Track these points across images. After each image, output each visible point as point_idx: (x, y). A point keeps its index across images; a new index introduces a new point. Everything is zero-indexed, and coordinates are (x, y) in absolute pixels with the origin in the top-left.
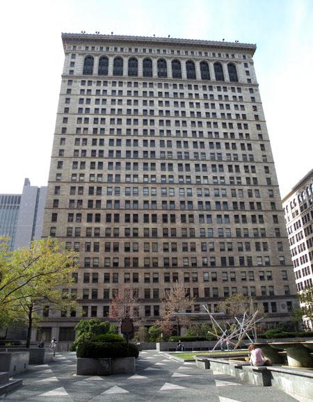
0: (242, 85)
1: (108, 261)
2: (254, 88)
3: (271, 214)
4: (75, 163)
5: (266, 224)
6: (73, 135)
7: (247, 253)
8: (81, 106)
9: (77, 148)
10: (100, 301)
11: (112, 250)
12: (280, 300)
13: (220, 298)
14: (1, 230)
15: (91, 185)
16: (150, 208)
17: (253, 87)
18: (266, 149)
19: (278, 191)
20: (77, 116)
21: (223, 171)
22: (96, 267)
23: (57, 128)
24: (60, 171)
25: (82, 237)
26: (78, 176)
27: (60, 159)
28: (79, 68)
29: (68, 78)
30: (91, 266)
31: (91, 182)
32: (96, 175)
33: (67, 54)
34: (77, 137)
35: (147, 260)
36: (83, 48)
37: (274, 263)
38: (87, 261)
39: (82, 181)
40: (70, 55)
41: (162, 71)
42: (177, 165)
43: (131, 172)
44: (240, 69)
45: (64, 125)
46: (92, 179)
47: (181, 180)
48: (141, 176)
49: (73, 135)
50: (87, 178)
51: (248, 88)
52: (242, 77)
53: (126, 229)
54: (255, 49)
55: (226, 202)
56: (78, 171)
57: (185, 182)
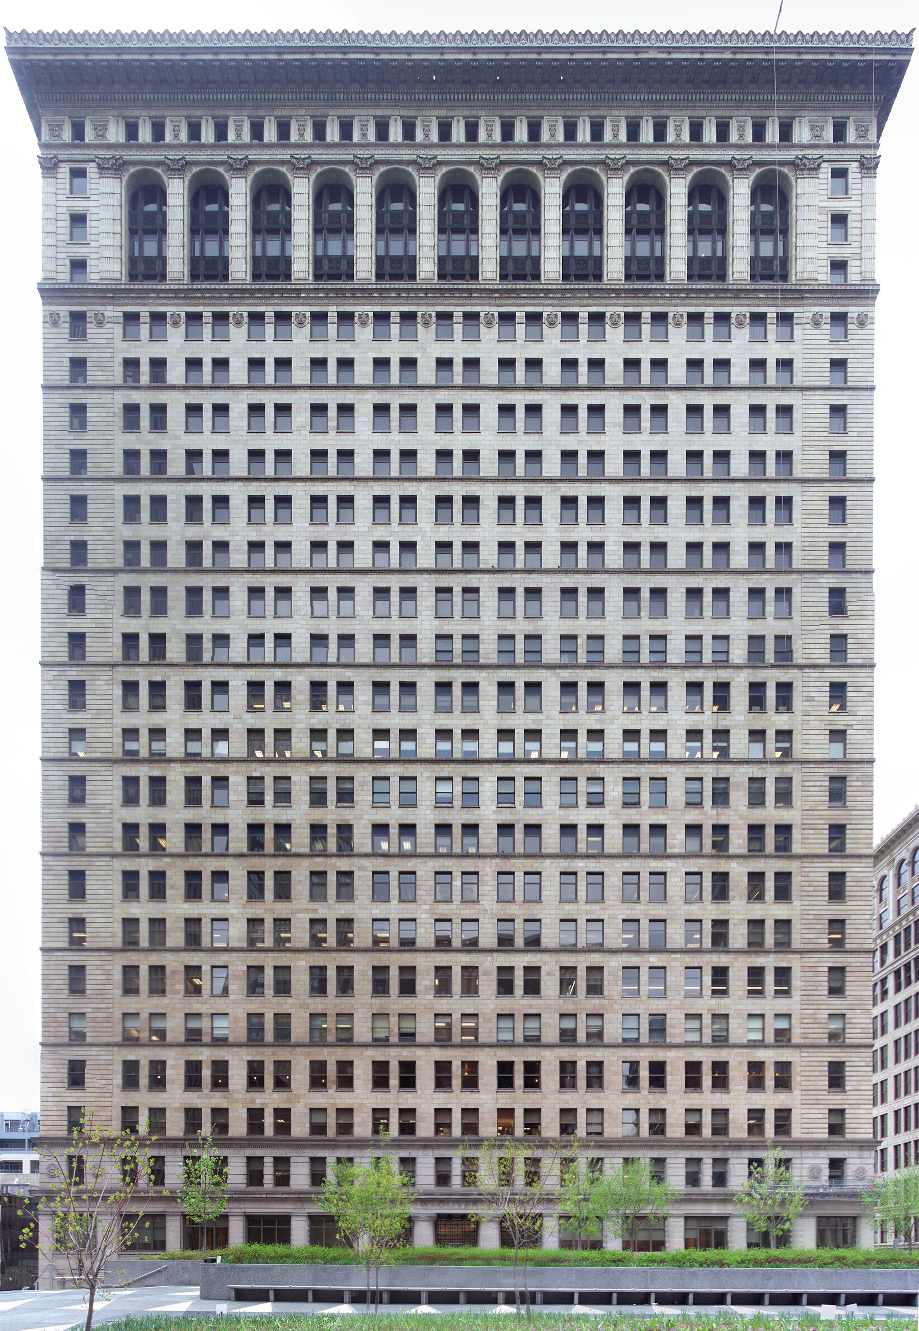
0: (802, 294)
1: (380, 1024)
2: (853, 311)
3: (821, 870)
4: (130, 687)
5: (796, 903)
6: (115, 571)
7: (713, 1002)
8: (131, 441)
9: (131, 625)
10: (175, 1143)
11: (269, 991)
12: (805, 1154)
13: (546, 1140)
14: (872, 912)
15: (192, 770)
16: (519, 849)
17: (848, 297)
18: (852, 606)
19: (868, 780)
20: (122, 490)
21: (414, 709)
22: (220, 1042)
23: (50, 545)
24: (78, 719)
25: (173, 950)
26: (144, 736)
27: (74, 674)
28: (108, 261)
29: (71, 300)
30: (206, 1039)
31: (192, 758)
32: (206, 734)
33: (49, 167)
34: (131, 580)
35: (632, 1023)
36: (116, 133)
37: (804, 1036)
38: (193, 1024)
39: (158, 758)
40: (64, 171)
41: (458, 249)
42: (494, 689)
43: (206, 720)
44: (811, 197)
45: (76, 533)
46: (194, 747)
47: (632, 747)
48: (363, 736)
49: (115, 571)
50: (174, 744)
51: (826, 311)
52: (810, 258)
53: (312, 921)
54: (901, 68)
55: (663, 827)
56: (143, 719)
57: (144, 753)
